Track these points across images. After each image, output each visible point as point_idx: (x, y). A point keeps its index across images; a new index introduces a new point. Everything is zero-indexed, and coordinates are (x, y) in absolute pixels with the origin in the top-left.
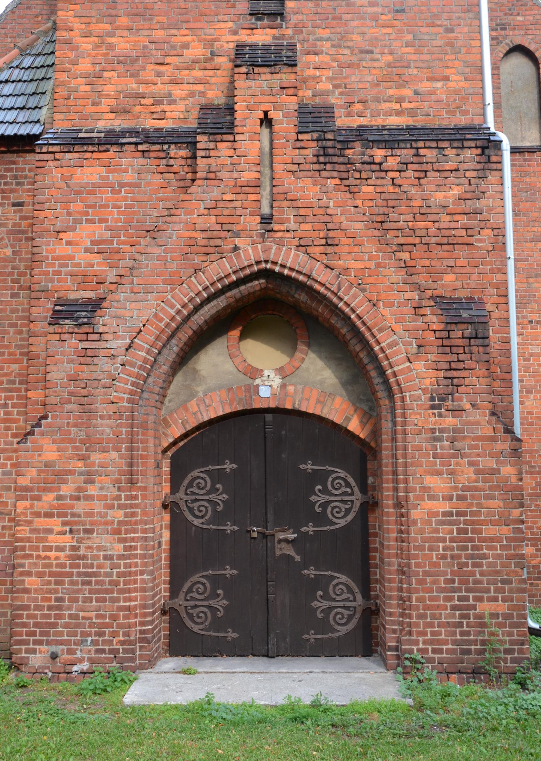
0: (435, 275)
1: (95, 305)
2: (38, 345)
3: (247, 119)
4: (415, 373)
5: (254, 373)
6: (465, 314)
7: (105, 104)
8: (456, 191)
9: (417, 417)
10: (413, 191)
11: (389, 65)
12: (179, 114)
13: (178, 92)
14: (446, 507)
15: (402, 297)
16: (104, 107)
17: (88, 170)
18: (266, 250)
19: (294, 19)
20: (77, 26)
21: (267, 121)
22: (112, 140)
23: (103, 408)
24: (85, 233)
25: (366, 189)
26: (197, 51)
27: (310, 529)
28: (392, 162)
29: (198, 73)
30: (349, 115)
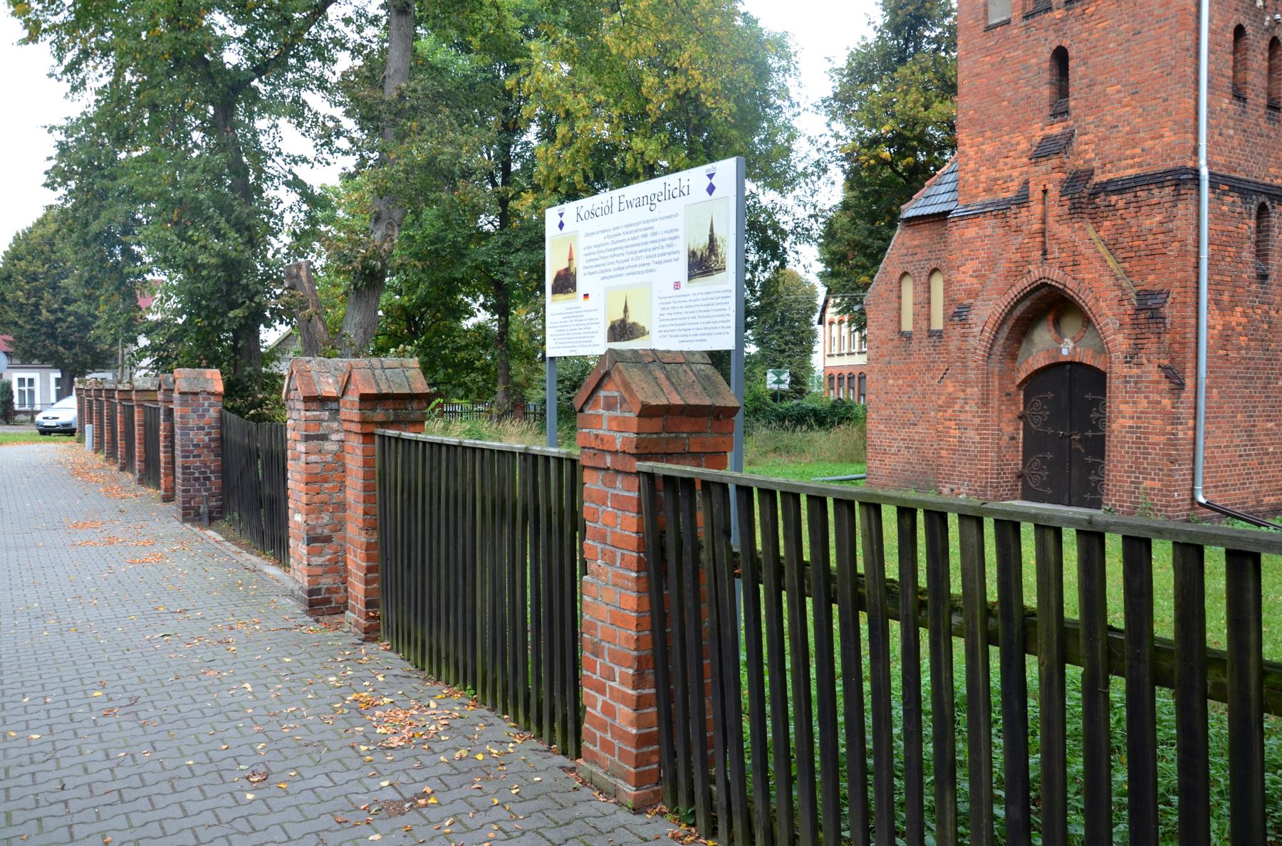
0: (1143, 276)
3: (1036, 194)
7: (982, 186)
8: (1158, 218)
11: (1128, 133)
13: (1015, 173)
14: (1130, 423)
15: (1113, 294)
16: (981, 189)
18: (1044, 271)
19: (1074, 113)
25: (1106, 223)
27: (1089, 434)
28: (1121, 204)
30: (1103, 172)
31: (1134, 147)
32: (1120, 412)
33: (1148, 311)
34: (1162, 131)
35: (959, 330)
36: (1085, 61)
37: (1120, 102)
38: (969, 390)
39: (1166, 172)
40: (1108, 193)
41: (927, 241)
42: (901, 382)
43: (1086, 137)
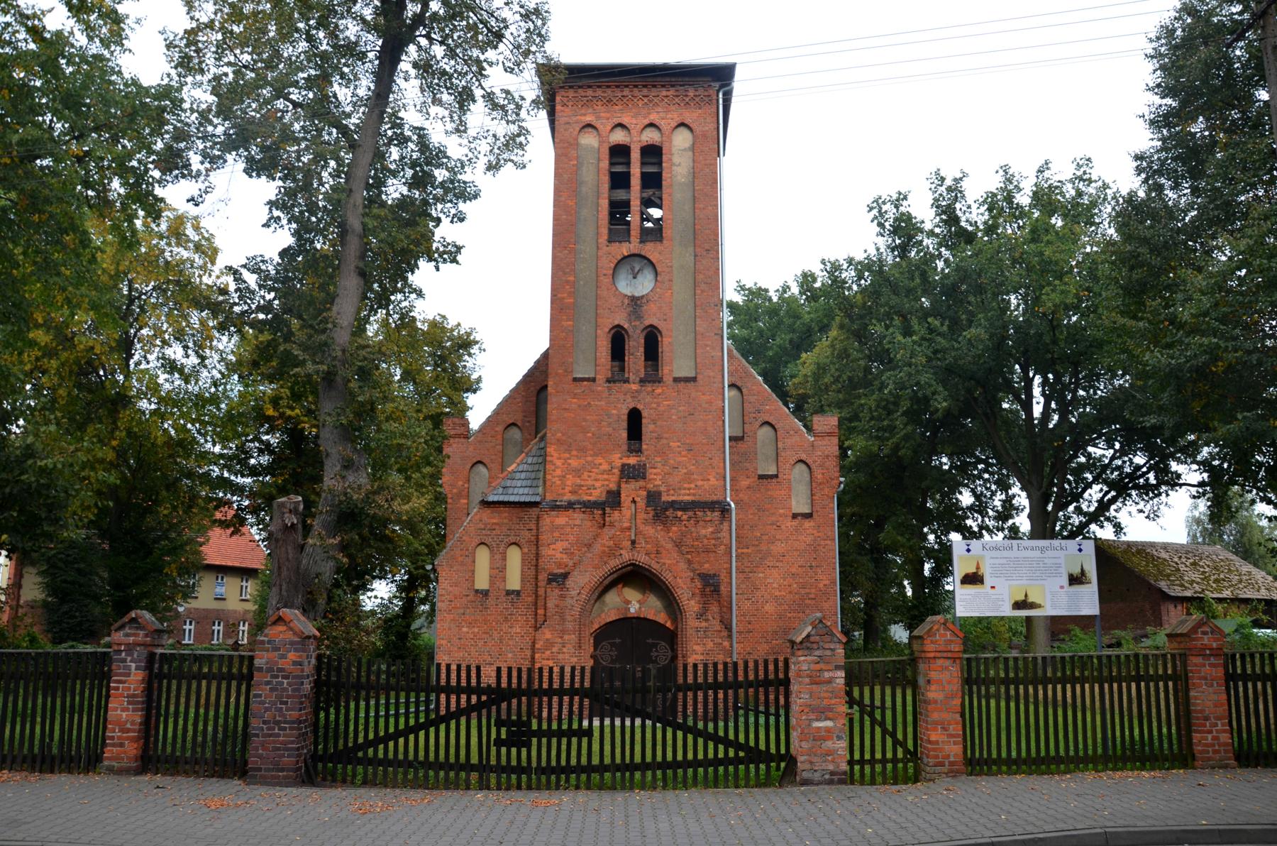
1: (565, 576)
4: (691, 605)
5: (628, 602)
7: (568, 489)
9: (691, 622)
12: (597, 494)
13: (597, 484)
21: (634, 501)
22: (570, 506)
23: (569, 618)
24: (560, 545)
26: (605, 467)
28: (685, 517)
38: (566, 637)
39: (713, 503)
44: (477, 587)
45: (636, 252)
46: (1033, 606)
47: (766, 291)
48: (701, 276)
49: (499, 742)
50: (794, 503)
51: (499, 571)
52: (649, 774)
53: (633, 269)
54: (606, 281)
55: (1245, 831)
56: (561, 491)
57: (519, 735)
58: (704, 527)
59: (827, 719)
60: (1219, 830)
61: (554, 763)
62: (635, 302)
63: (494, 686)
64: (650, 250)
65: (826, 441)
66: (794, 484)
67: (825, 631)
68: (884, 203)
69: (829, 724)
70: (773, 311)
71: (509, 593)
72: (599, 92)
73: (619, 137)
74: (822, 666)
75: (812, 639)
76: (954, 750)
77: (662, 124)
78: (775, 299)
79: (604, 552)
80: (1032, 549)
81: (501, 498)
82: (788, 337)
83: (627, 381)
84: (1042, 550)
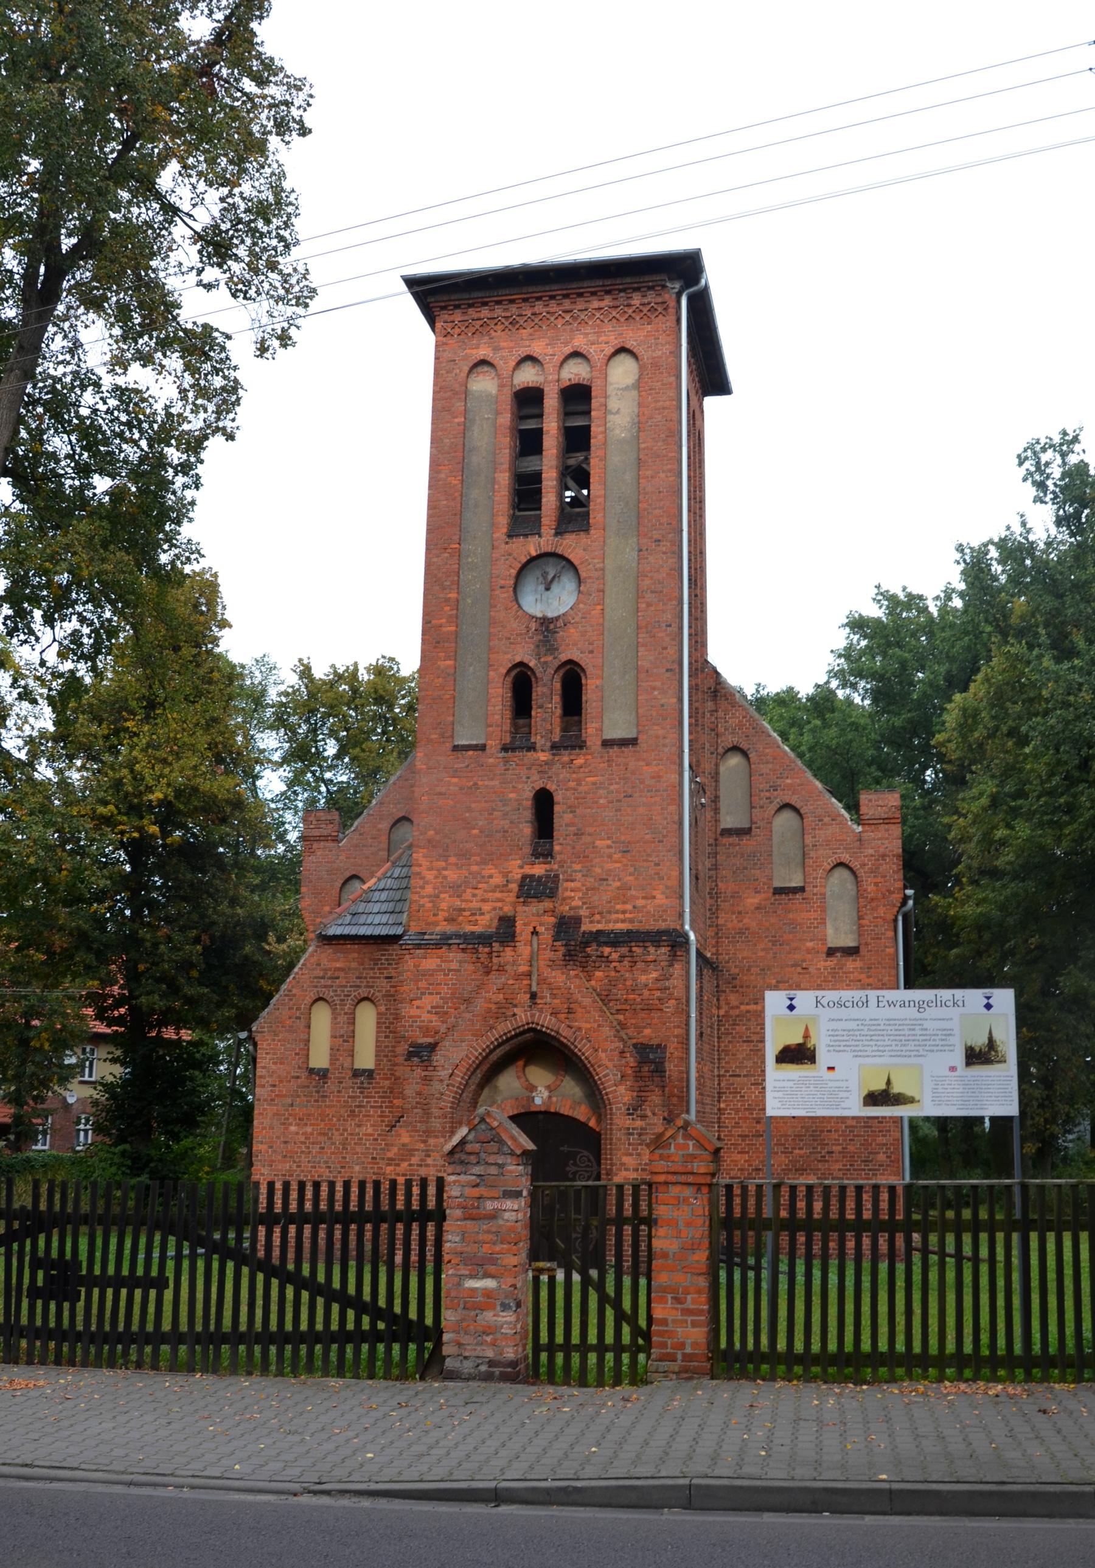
0: (639, 1029)
1: (432, 1047)
2: (400, 1071)
3: (522, 929)
4: (620, 1094)
5: (532, 1088)
6: (651, 1056)
7: (442, 915)
8: (654, 975)
9: (620, 1120)
10: (627, 975)
12: (485, 923)
13: (486, 907)
17: (429, 961)
18: (533, 1016)
19: (558, 858)
20: (425, 863)
21: (535, 932)
22: (444, 942)
23: (435, 1111)
24: (428, 1001)
26: (498, 880)
28: (615, 956)
29: (498, 895)
31: (624, 903)
32: (623, 1164)
33: (649, 1063)
34: (655, 893)
35: (419, 1072)
36: (572, 809)
37: (610, 856)
39: (660, 933)
40: (600, 944)
41: (354, 965)
42: (309, 1129)
43: (572, 884)
44: (356, 1066)
45: (549, 549)
46: (899, 1100)
47: (921, 597)
48: (647, 582)
49: (35, 1293)
50: (830, 931)
51: (344, 1040)
52: (183, 1348)
53: (545, 575)
54: (506, 595)
55: (937, 1493)
56: (432, 919)
57: (63, 1281)
58: (644, 971)
59: (487, 1275)
60: (890, 1491)
61: (289, 1327)
62: (547, 626)
63: (30, 1207)
64: (572, 546)
65: (882, 831)
66: (830, 901)
67: (489, 1135)
68: (1044, 450)
69: (490, 1283)
70: (930, 627)
71: (357, 1073)
72: (499, 311)
73: (528, 376)
74: (482, 1191)
75: (469, 1147)
76: (691, 1335)
77: (592, 351)
78: (934, 610)
79: (489, 1010)
80: (903, 1005)
81: (347, 931)
82: (943, 669)
83: (532, 748)
84: (920, 1006)
